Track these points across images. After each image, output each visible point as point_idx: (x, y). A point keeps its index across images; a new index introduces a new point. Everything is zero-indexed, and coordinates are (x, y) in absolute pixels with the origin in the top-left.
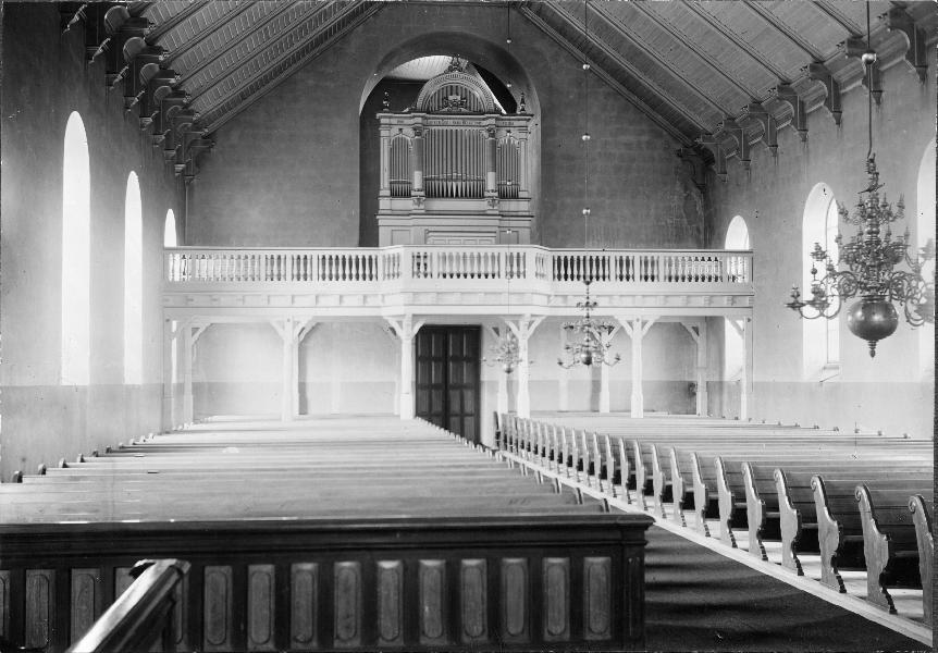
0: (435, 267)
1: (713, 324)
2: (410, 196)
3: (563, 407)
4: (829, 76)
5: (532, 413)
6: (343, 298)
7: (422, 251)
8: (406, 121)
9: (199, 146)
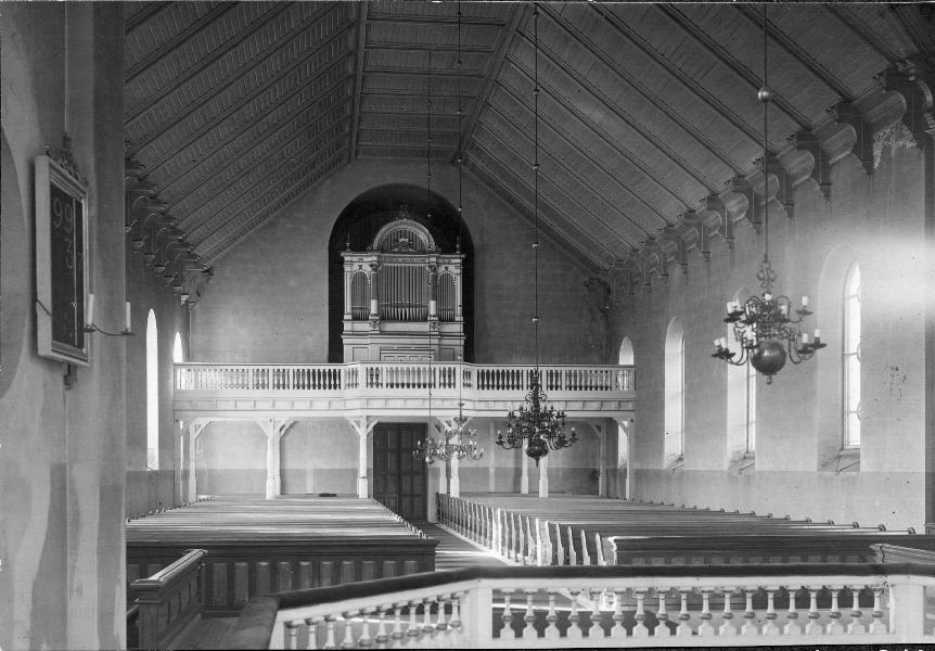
0: (384, 379)
1: (611, 425)
2: (367, 319)
3: (492, 488)
4: (751, 189)
5: (461, 494)
6: (316, 404)
7: (375, 366)
8: (365, 259)
9: (198, 281)
